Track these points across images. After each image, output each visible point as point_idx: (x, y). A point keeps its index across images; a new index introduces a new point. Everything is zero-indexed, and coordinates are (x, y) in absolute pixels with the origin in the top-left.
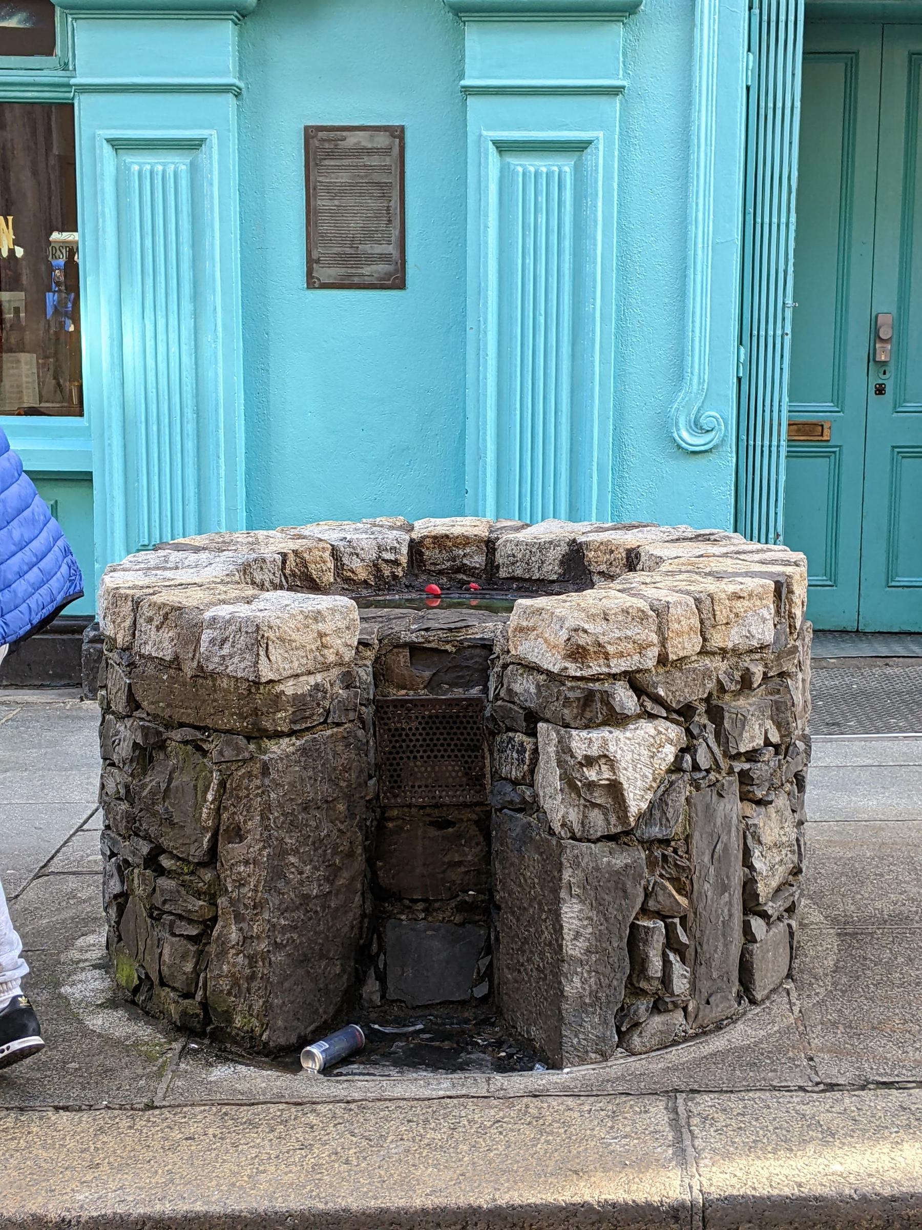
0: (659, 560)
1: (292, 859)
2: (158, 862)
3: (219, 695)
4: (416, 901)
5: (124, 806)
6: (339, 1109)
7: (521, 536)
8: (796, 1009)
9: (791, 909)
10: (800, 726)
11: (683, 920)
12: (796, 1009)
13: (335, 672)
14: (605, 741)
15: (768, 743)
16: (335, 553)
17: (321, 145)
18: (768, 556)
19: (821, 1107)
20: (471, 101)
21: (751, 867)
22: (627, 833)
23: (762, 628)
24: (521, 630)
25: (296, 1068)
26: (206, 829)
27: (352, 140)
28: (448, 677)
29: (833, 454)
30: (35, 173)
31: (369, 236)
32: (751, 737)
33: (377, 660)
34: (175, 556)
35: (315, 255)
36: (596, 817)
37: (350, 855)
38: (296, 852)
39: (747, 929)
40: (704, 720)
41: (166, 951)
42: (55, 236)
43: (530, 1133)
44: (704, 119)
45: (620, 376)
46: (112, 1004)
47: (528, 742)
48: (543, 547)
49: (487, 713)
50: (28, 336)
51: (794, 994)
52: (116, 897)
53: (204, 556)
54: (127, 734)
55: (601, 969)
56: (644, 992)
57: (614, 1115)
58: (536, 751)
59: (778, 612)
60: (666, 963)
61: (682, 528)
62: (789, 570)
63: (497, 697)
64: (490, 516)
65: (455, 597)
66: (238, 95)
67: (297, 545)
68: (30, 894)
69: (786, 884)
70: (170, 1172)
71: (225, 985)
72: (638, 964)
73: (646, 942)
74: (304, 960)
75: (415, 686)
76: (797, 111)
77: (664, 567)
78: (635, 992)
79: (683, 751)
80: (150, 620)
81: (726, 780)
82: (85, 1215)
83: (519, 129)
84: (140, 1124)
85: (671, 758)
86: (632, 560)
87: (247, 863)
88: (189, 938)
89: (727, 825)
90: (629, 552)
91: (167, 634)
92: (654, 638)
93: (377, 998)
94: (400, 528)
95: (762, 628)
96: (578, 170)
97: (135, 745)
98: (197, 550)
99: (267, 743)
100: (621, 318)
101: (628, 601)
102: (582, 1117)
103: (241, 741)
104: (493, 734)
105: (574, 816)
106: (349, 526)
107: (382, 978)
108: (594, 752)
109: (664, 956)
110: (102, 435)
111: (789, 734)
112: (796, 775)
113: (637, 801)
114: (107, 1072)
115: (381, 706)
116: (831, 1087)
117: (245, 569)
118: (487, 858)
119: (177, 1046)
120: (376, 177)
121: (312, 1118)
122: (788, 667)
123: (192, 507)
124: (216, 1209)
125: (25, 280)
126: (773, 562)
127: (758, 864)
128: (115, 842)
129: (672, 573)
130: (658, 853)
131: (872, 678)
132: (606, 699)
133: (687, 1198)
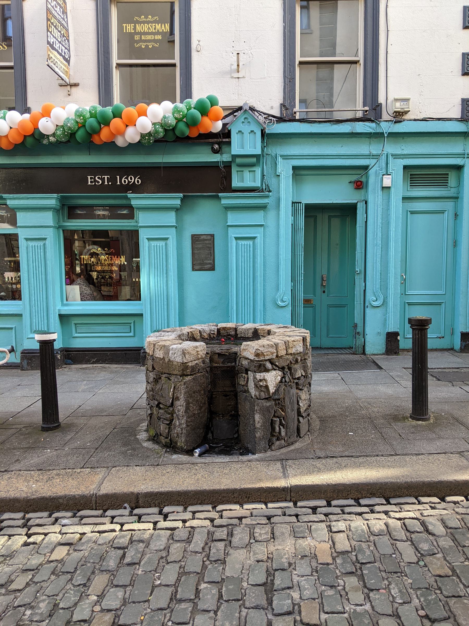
0: (275, 333)
1: (191, 405)
2: (159, 405)
3: (174, 366)
4: (220, 414)
5: (151, 393)
6: (203, 465)
7: (243, 327)
8: (310, 439)
9: (308, 415)
10: (309, 371)
11: (284, 418)
12: (310, 439)
13: (201, 360)
14: (264, 376)
15: (302, 375)
16: (200, 332)
17: (195, 238)
18: (301, 331)
19: (318, 463)
20: (229, 228)
21: (299, 405)
22: (270, 398)
23: (300, 349)
24: (244, 349)
25: (192, 455)
26: (171, 398)
27: (202, 237)
28: (227, 361)
29: (314, 307)
30: (129, 245)
31: (206, 259)
32: (298, 374)
33: (210, 357)
34: (163, 333)
35: (194, 263)
36: (262, 394)
37: (205, 403)
38: (192, 403)
39: (298, 419)
40: (287, 370)
41: (161, 427)
42: (134, 259)
43: (248, 470)
44: (282, 231)
45: (264, 289)
46: (149, 440)
47: (246, 376)
48: (248, 330)
49: (236, 369)
50: (128, 282)
51: (310, 435)
52: (149, 414)
53: (170, 333)
54: (152, 376)
55: (264, 430)
56: (275, 436)
57: (268, 466)
58: (248, 378)
59: (303, 344)
60: (280, 429)
61: (280, 325)
62: (306, 335)
63: (238, 365)
64: (235, 323)
65: (228, 342)
66: (176, 228)
67: (191, 330)
68: (129, 414)
69: (307, 409)
70: (163, 481)
71: (175, 435)
72: (273, 429)
73: (275, 424)
74: (194, 429)
75: (219, 363)
76: (303, 229)
77: (277, 334)
78: (272, 436)
79: (282, 378)
80: (158, 349)
81: (293, 384)
82: (143, 492)
83: (240, 234)
84: (156, 469)
85: (280, 379)
86: (269, 333)
87: (180, 406)
88: (167, 424)
89: (293, 394)
90: (268, 330)
91: (161, 352)
92: (275, 351)
93: (211, 438)
94: (215, 326)
95: (300, 349)
96: (253, 243)
97: (154, 378)
98: (168, 332)
99: (185, 377)
100: (264, 276)
101: (268, 342)
102: (261, 467)
103: (179, 377)
104: (238, 374)
105: (257, 393)
106: (203, 325)
107: (212, 433)
108: (262, 378)
109: (279, 427)
110: (145, 305)
111: (307, 373)
112: (309, 383)
113: (272, 389)
114: (148, 457)
115: (211, 368)
116: (319, 458)
117: (179, 336)
118: (237, 404)
119: (164, 450)
120: (208, 246)
121: (197, 467)
122: (306, 357)
123: (166, 321)
124: (174, 490)
125: (127, 269)
126: (302, 333)
127: (301, 404)
128: (149, 401)
129: (279, 336)
130: (277, 402)
131: (324, 359)
132: (264, 366)
133: (286, 485)
